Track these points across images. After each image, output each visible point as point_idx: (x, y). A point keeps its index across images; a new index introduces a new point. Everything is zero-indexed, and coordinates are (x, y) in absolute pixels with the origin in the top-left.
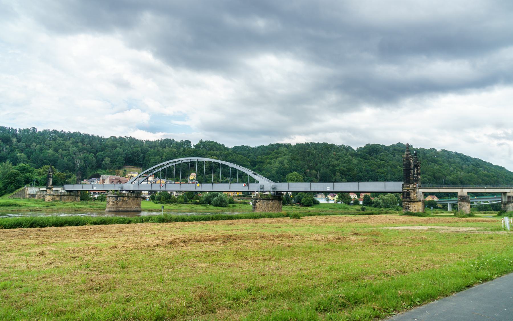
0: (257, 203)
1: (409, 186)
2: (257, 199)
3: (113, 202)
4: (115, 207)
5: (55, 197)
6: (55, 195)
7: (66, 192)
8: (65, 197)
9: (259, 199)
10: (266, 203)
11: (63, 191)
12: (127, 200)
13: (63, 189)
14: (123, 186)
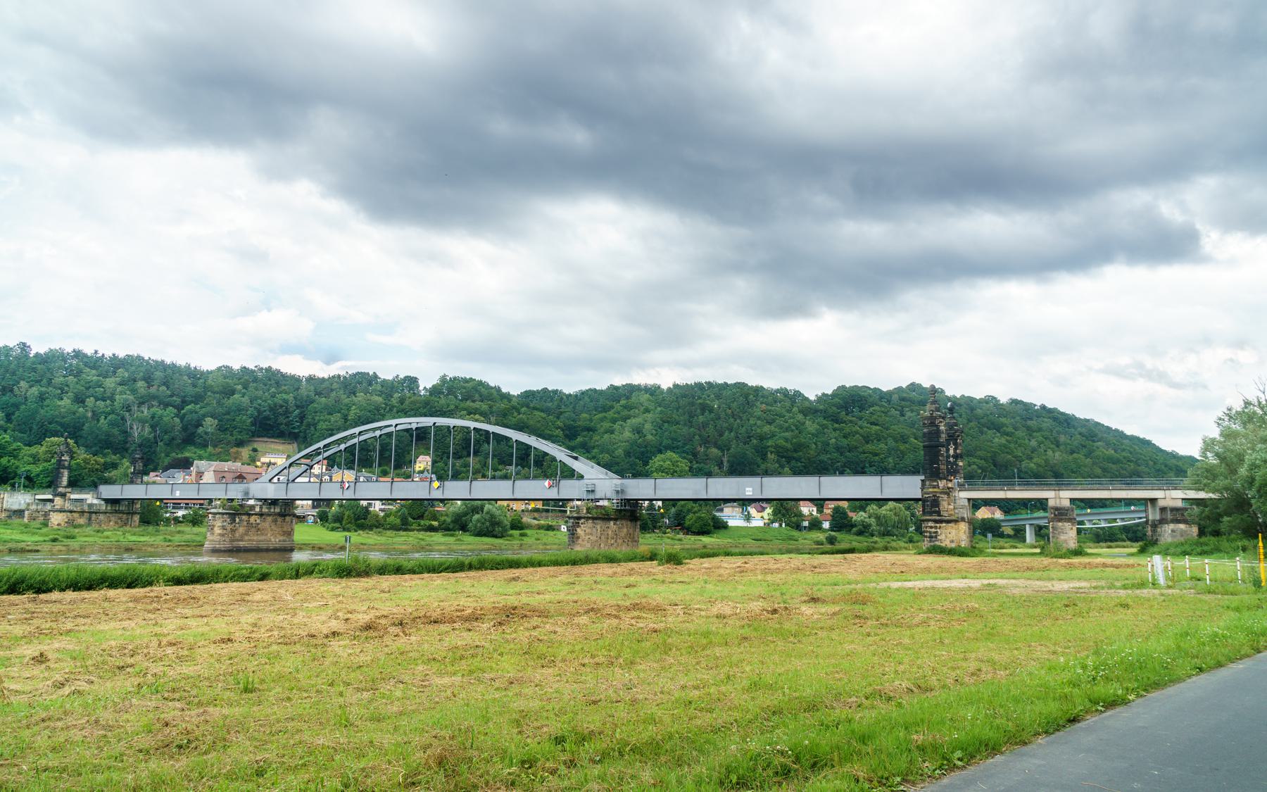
0: (579, 526)
1: (938, 485)
2: (579, 518)
3: (223, 528)
4: (227, 540)
5: (76, 515)
6: (75, 512)
7: (103, 502)
8: (102, 517)
9: (584, 518)
10: (601, 527)
11: (95, 501)
12: (258, 521)
13: (95, 496)
14: (248, 488)
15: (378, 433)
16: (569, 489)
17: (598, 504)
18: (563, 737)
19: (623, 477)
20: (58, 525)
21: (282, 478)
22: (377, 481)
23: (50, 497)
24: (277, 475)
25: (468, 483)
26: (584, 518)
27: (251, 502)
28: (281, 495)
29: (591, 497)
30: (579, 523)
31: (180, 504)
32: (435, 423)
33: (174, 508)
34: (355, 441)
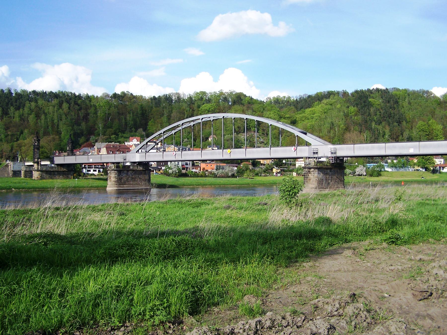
2: (310, 168)
9: (313, 168)
15: (192, 124)
16: (303, 151)
17: (320, 160)
18: (297, 311)
19: (333, 144)
20: (37, 178)
21: (143, 150)
22: (193, 150)
23: (32, 164)
24: (140, 149)
25: (222, 150)
26: (313, 168)
27: (128, 164)
28: (143, 160)
29: (316, 156)
30: (310, 171)
31: (91, 166)
32: (224, 117)
33: (89, 168)
34: (180, 128)
